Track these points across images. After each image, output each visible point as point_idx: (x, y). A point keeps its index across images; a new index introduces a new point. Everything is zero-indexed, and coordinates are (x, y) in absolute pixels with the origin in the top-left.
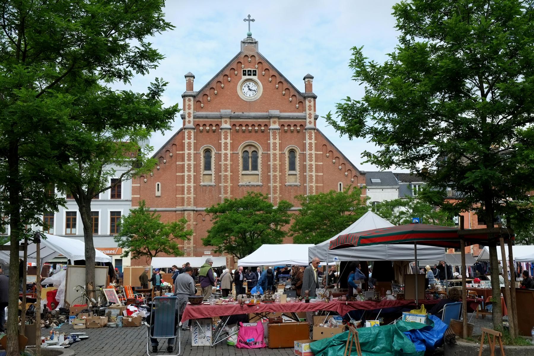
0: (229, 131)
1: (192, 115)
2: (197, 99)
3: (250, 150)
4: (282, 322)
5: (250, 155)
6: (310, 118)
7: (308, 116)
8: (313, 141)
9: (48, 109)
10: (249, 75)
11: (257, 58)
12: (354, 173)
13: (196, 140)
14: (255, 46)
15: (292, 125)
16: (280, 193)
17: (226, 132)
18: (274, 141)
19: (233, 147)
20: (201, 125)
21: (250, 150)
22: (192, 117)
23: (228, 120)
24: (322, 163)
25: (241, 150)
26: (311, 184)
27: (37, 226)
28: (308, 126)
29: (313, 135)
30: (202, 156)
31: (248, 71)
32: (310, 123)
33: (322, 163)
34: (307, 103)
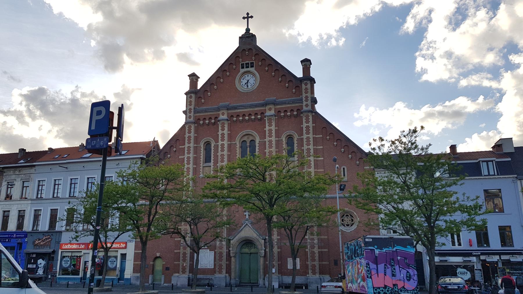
0: (226, 122)
2: (199, 95)
3: (248, 140)
4: (379, 235)
5: (248, 144)
7: (304, 99)
8: (311, 124)
9: (223, 113)
10: (247, 67)
11: (254, 50)
12: (359, 155)
14: (252, 40)
15: (289, 111)
17: (223, 124)
20: (201, 119)
21: (248, 140)
22: (192, 113)
23: (225, 112)
24: (322, 147)
25: (238, 140)
26: (310, 170)
27: (438, 124)
28: (305, 108)
29: (311, 118)
30: (202, 149)
32: (307, 105)
33: (322, 147)
34: (304, 86)
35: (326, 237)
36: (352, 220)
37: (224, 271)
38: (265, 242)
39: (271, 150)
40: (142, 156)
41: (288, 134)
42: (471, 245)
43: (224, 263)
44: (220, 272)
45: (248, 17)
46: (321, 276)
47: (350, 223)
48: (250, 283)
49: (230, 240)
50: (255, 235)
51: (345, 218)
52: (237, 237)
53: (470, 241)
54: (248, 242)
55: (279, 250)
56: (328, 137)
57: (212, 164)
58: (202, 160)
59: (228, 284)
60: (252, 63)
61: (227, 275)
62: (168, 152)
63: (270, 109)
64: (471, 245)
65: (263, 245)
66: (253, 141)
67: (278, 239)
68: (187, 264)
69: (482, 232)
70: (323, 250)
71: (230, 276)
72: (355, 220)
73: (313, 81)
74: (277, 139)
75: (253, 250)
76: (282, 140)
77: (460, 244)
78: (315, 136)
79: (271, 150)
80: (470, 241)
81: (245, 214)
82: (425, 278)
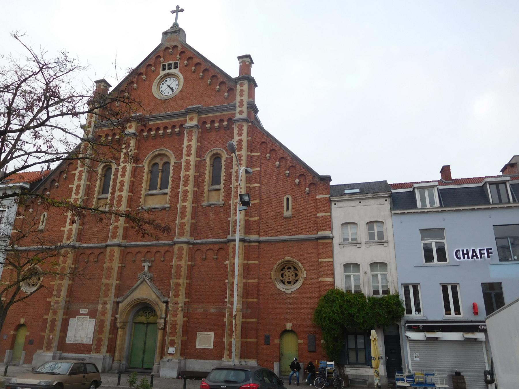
1: (245, 103)
3: (160, 162)
5: (160, 168)
6: (241, 105)
7: (238, 104)
13: (201, 143)
16: (193, 218)
18: (190, 143)
19: (200, 152)
21: (160, 162)
25: (147, 162)
28: (238, 116)
31: (169, 65)
34: (238, 88)
35: (255, 300)
36: (296, 275)
37: (104, 349)
38: (167, 307)
39: (188, 173)
40: (21, 184)
41: (214, 152)
42: (476, 313)
43: (106, 337)
44: (98, 351)
45: (178, 10)
46: (242, 360)
47: (292, 278)
48: (142, 368)
49: (118, 303)
50: (154, 296)
51: (287, 272)
52: (129, 299)
53: (475, 307)
54: (145, 308)
55: (185, 319)
56: (268, 155)
57: (109, 195)
58: (97, 189)
59: (107, 370)
60: (176, 64)
61: (108, 355)
62: (57, 180)
63: (192, 119)
64: (476, 313)
65: (164, 311)
66: (167, 163)
67: (186, 303)
68: (55, 337)
69: (493, 293)
70: (249, 320)
71: (113, 356)
72: (300, 274)
73: (252, 83)
74: (198, 159)
75: (151, 319)
76: (205, 160)
77: (457, 310)
78: (249, 153)
79: (188, 173)
80: (475, 307)
81: (144, 264)
82: (403, 366)
